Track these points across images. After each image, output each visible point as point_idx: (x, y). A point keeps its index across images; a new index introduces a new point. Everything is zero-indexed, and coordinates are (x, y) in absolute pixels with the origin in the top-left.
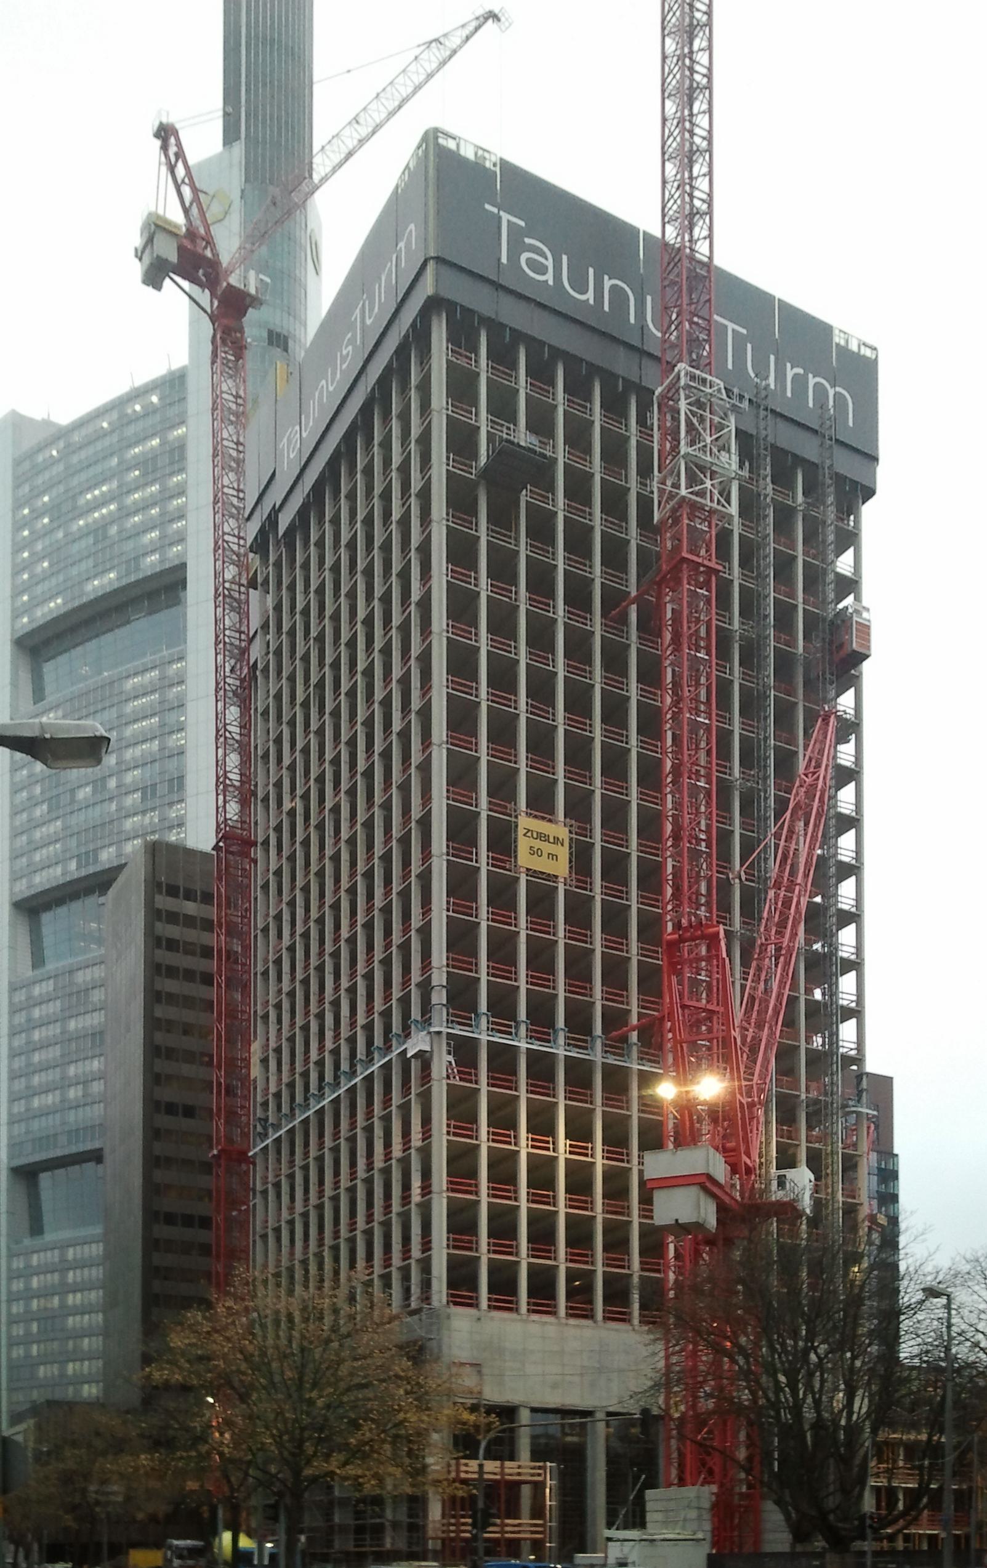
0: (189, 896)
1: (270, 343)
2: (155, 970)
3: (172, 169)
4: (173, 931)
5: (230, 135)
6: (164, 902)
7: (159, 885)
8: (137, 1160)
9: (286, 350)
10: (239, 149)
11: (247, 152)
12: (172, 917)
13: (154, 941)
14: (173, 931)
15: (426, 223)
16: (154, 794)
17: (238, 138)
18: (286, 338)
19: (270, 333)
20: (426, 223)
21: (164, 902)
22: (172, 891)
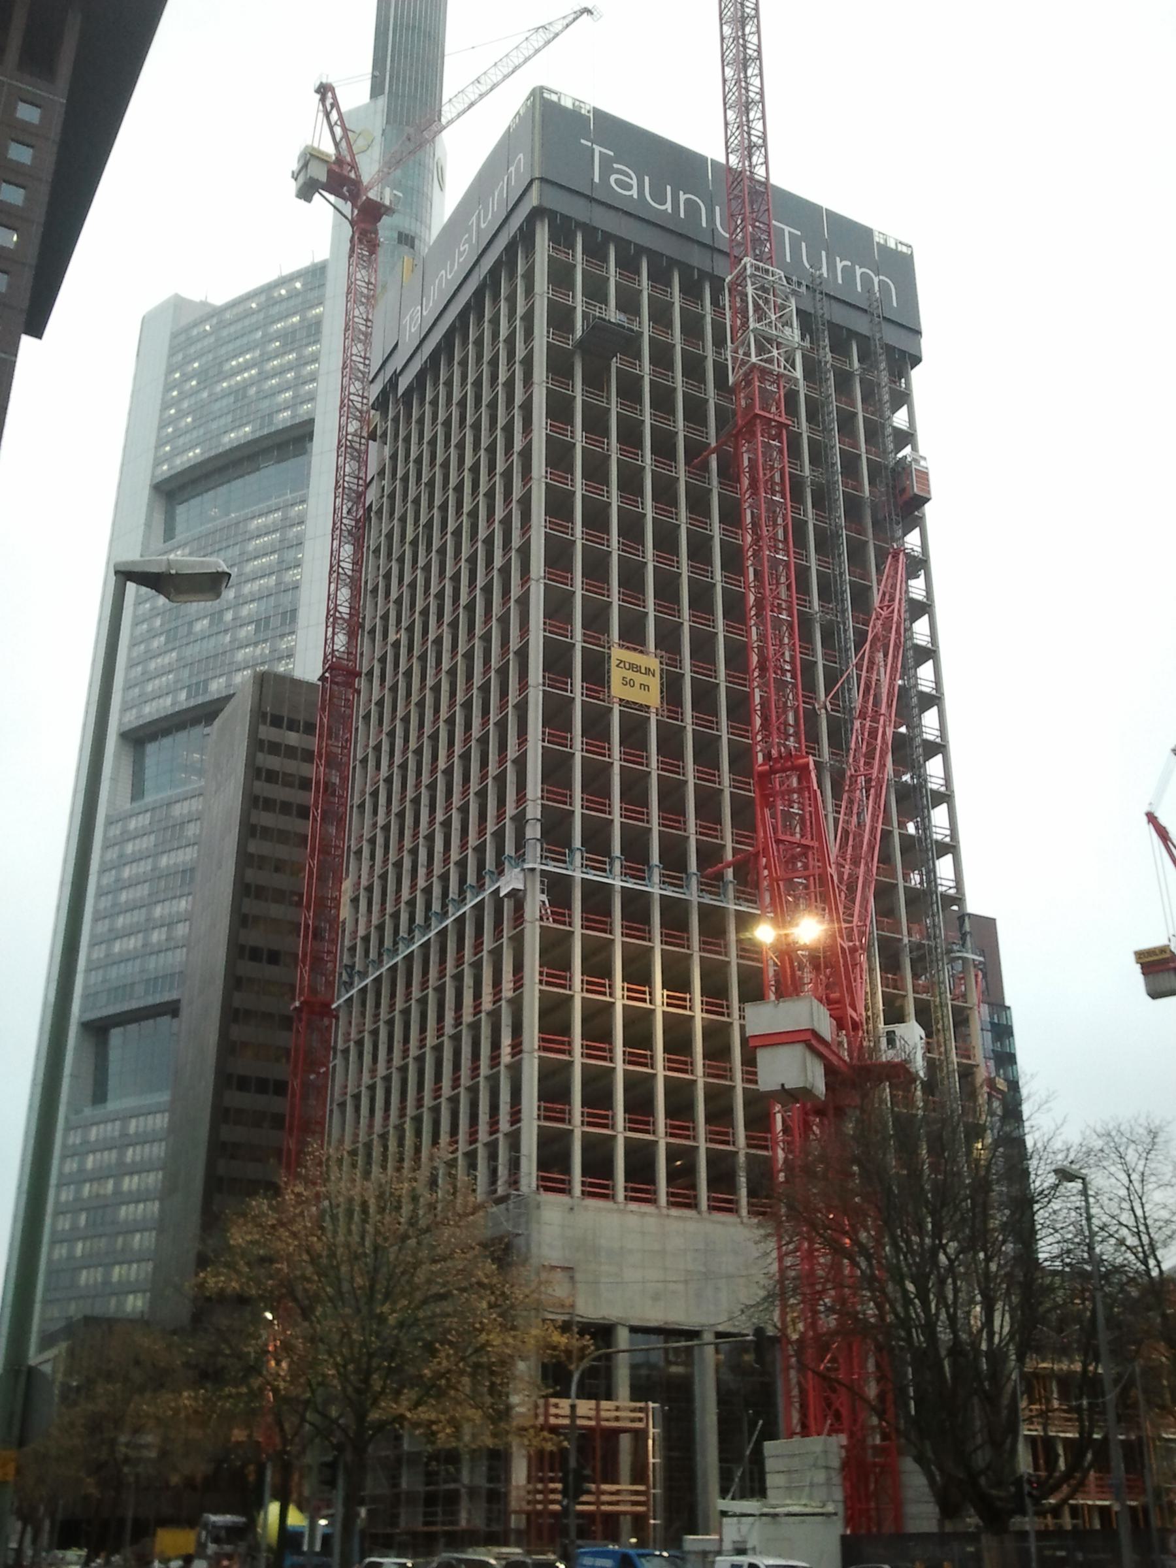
0: (292, 726)
3: (327, 115)
6: (267, 733)
7: (264, 715)
9: (412, 247)
18: (413, 239)
22: (277, 721)
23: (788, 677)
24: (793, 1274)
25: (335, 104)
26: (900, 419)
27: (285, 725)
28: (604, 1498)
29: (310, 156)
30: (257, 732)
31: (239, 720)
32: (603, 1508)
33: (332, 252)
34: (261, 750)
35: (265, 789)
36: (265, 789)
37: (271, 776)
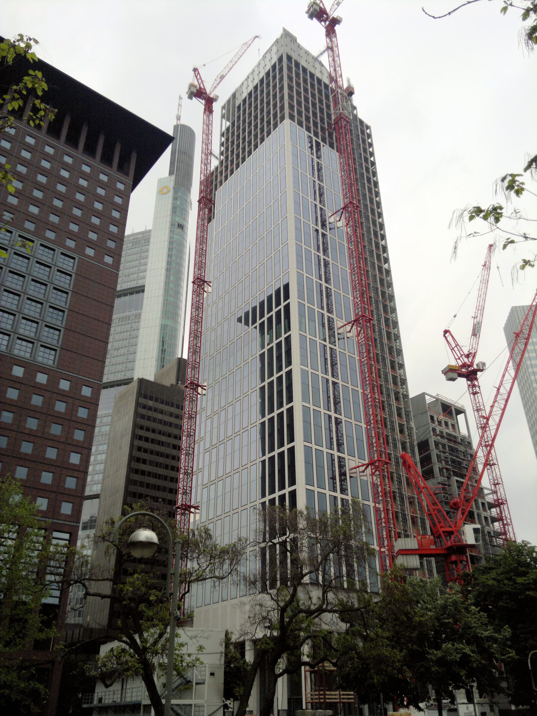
0: (151, 399)
1: (178, 227)
2: (136, 426)
3: (196, 77)
4: (144, 412)
5: (171, 173)
6: (142, 401)
7: (141, 394)
8: (121, 493)
9: (182, 229)
10: (173, 177)
11: (176, 179)
12: (144, 407)
13: (136, 414)
14: (144, 412)
15: (28, 337)
16: (129, 319)
17: (173, 174)
18: (183, 226)
19: (179, 224)
20: (28, 337)
21: (142, 401)
22: (145, 397)
23: (362, 272)
24: (451, 600)
25: (199, 73)
26: (223, 139)
27: (137, 497)
28: (327, 697)
29: (192, 85)
30: (132, 454)
31: (134, 386)
32: (327, 701)
33: (153, 227)
34: (138, 428)
35: (136, 477)
36: (136, 477)
37: (143, 417)
